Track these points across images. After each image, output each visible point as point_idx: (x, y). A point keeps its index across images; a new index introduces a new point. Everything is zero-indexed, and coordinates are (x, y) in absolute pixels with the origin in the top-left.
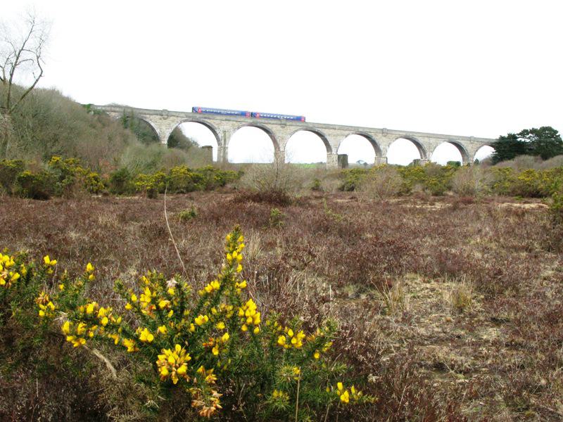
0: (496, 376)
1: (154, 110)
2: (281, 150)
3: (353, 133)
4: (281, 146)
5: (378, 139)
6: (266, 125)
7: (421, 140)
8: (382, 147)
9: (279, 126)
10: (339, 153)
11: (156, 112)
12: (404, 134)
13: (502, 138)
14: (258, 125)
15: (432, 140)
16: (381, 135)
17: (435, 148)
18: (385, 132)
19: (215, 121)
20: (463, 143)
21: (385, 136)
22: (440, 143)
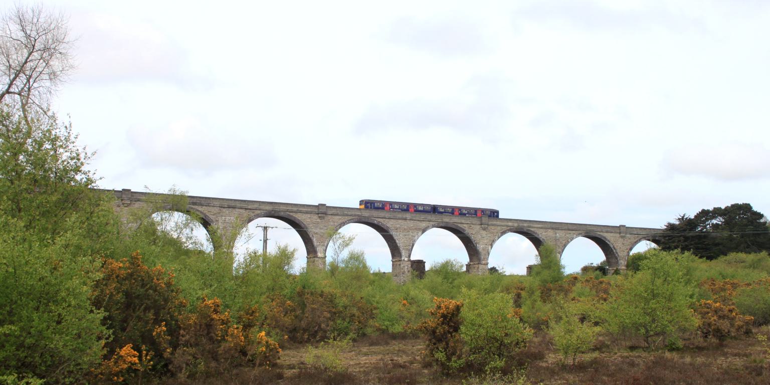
0: (705, 344)
1: (550, 222)
2: (320, 255)
3: (434, 226)
4: (320, 250)
5: (473, 230)
6: (459, 225)
7: (542, 234)
8: (480, 247)
9: (316, 217)
10: (413, 258)
11: (575, 227)
12: (516, 225)
13: (738, 204)
14: (282, 214)
15: (560, 234)
16: (479, 227)
17: (565, 246)
18: (322, 211)
19: (210, 209)
20: (609, 237)
21: (484, 229)
22: (572, 239)
